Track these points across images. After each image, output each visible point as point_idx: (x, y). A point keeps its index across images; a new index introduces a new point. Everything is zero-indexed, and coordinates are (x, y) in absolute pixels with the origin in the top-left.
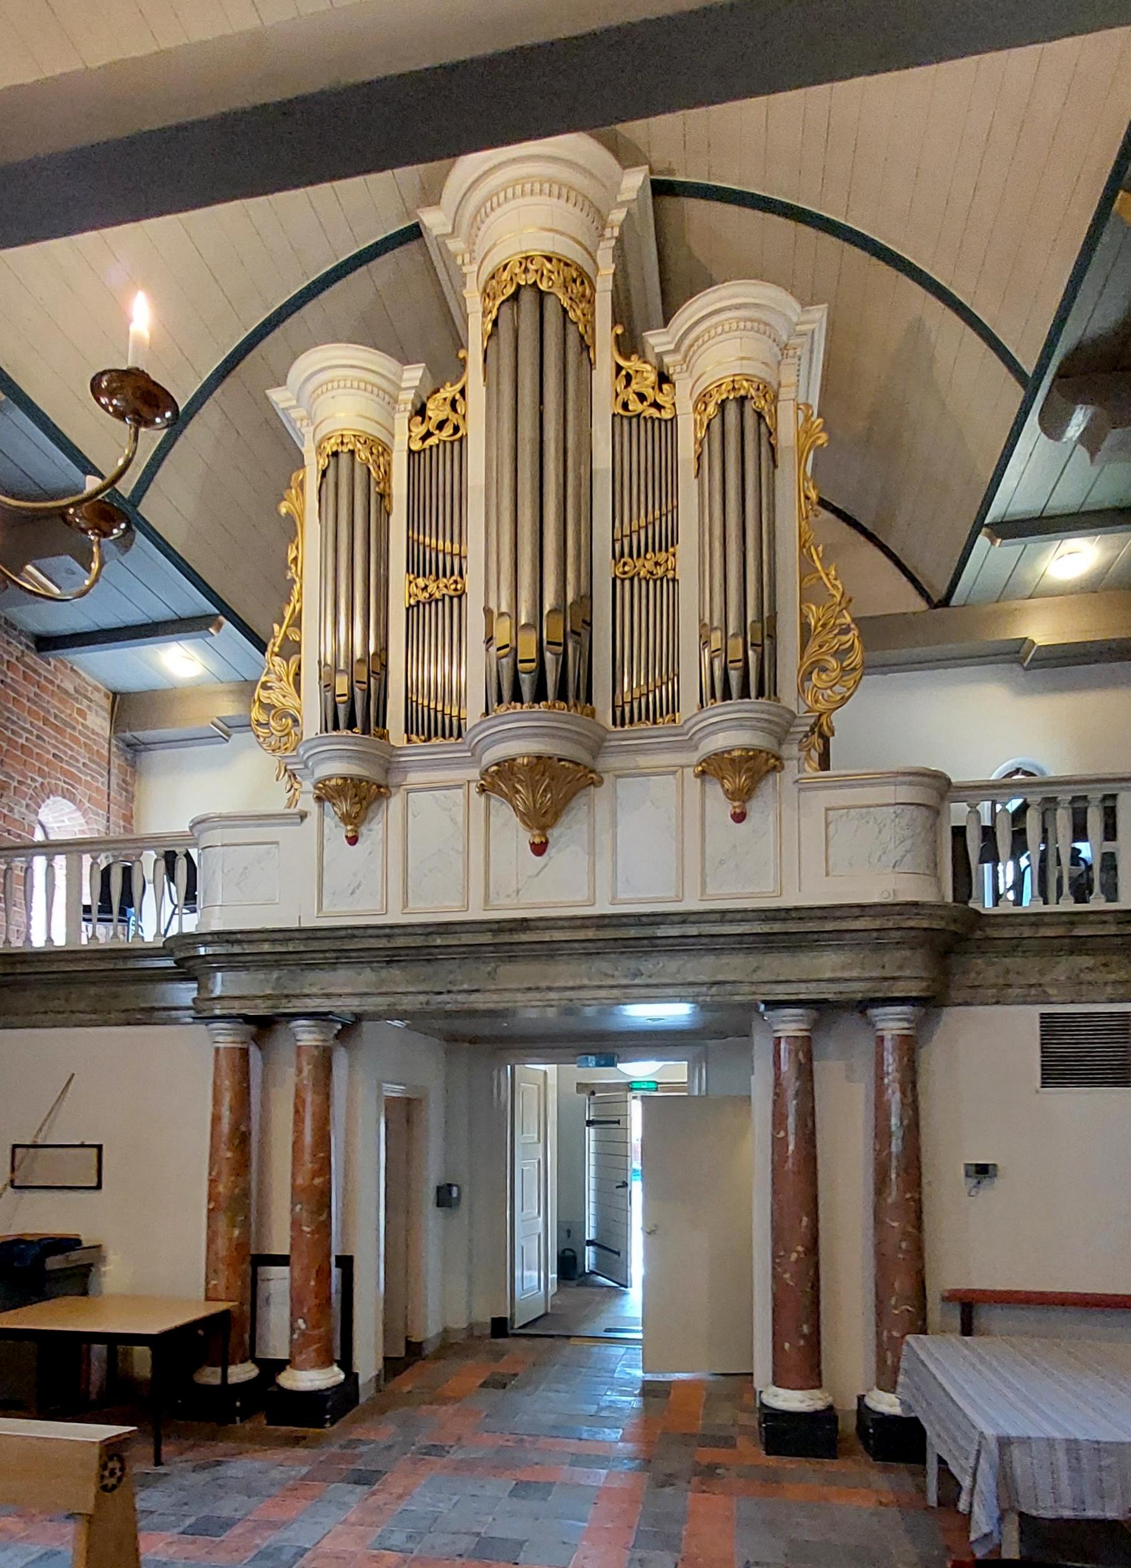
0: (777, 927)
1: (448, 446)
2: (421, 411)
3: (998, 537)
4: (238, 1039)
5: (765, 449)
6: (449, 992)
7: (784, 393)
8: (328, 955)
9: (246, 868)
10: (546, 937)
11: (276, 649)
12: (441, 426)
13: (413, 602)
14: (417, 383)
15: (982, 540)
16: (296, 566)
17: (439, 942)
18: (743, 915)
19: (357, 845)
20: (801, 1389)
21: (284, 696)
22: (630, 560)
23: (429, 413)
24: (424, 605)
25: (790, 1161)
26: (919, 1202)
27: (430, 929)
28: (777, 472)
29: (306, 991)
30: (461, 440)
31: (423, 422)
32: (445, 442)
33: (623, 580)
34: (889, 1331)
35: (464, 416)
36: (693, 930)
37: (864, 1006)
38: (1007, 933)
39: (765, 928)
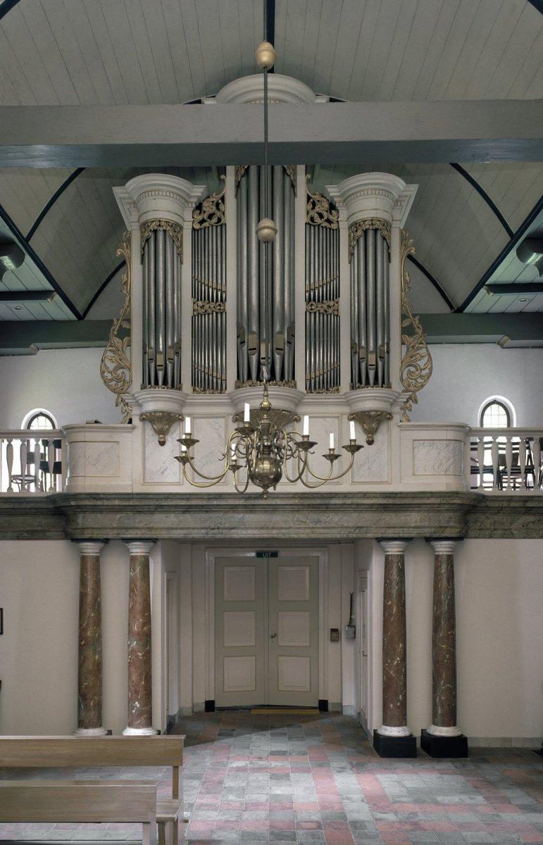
0: (390, 501)
1: (214, 228)
2: (199, 207)
3: (492, 292)
6: (218, 528)
7: (395, 225)
11: (116, 333)
12: (211, 216)
13: (196, 313)
14: (200, 194)
15: (483, 291)
16: (127, 286)
17: (215, 503)
19: (165, 446)
20: (398, 726)
21: (121, 360)
22: (314, 303)
23: (204, 209)
24: (201, 316)
26: (454, 636)
27: (211, 496)
28: (391, 265)
29: (137, 526)
30: (221, 226)
31: (200, 213)
32: (212, 226)
33: (310, 313)
34: (440, 697)
35: (224, 213)
36: (349, 502)
37: (429, 540)
38: (497, 505)
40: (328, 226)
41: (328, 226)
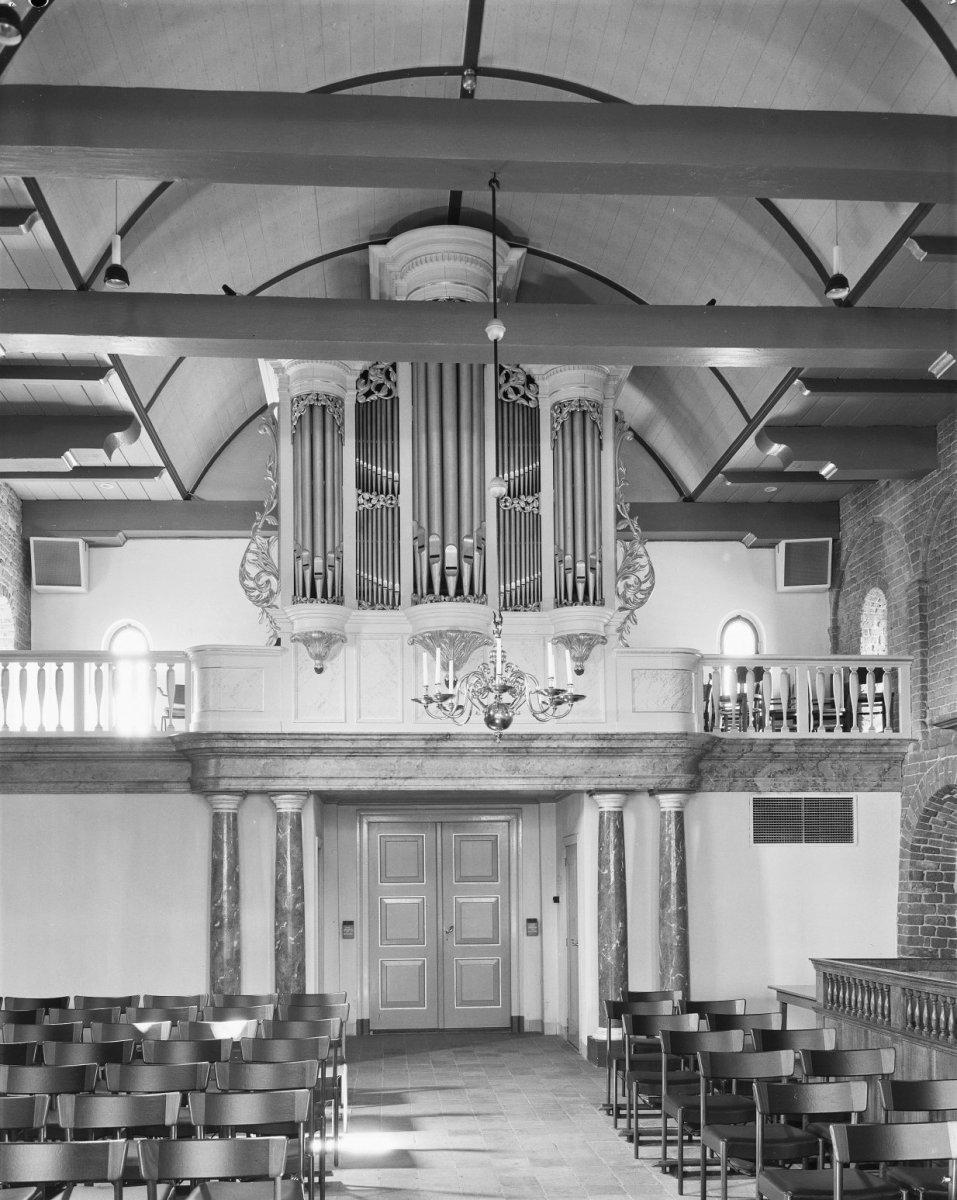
0: (605, 744)
4: (296, 806)
5: (596, 440)
8: (305, 751)
9: (238, 685)
10: (461, 744)
12: (379, 387)
17: (388, 745)
18: (586, 737)
25: (613, 887)
31: (366, 383)
36: (554, 744)
39: (598, 744)
40: (525, 403)
41: (525, 403)
